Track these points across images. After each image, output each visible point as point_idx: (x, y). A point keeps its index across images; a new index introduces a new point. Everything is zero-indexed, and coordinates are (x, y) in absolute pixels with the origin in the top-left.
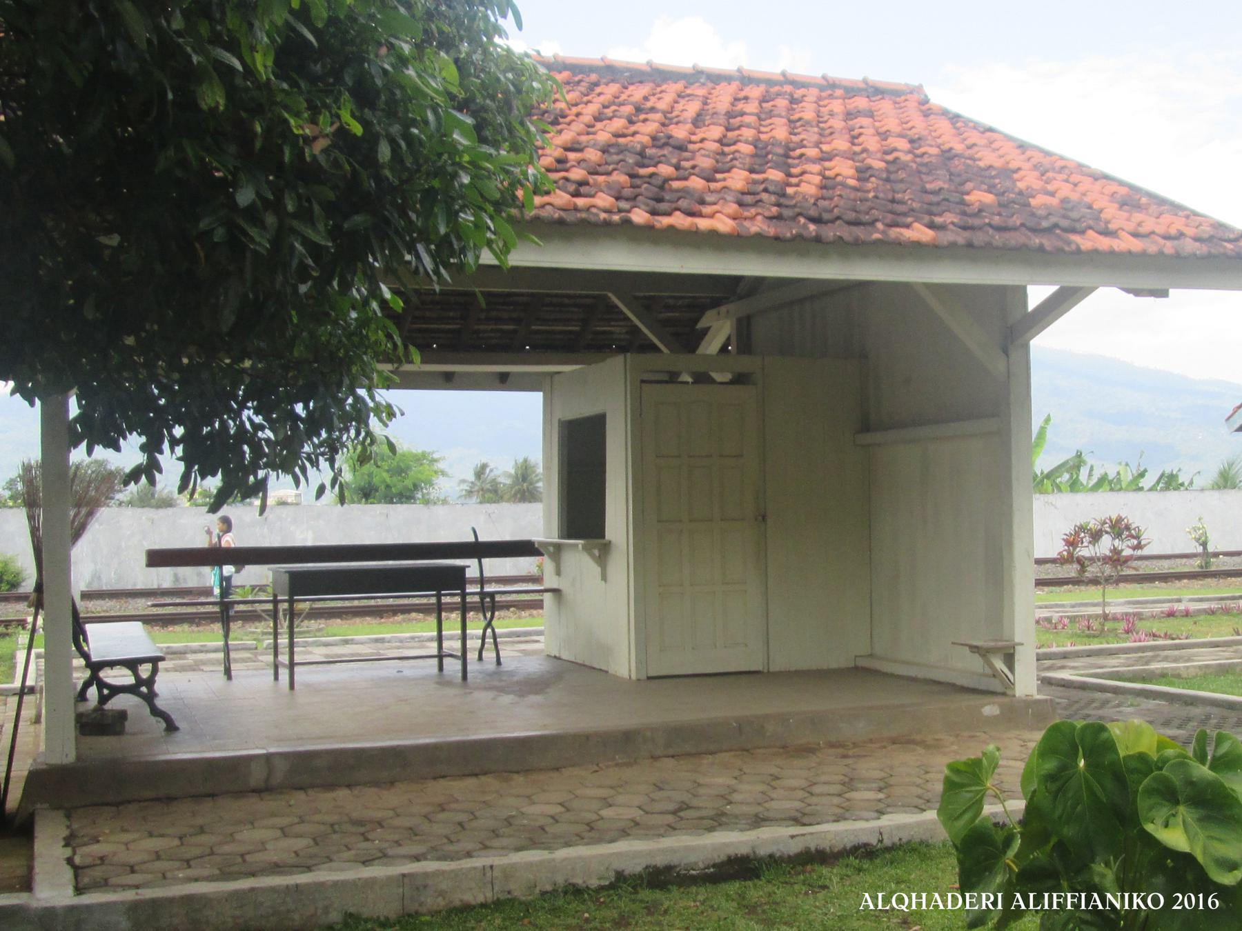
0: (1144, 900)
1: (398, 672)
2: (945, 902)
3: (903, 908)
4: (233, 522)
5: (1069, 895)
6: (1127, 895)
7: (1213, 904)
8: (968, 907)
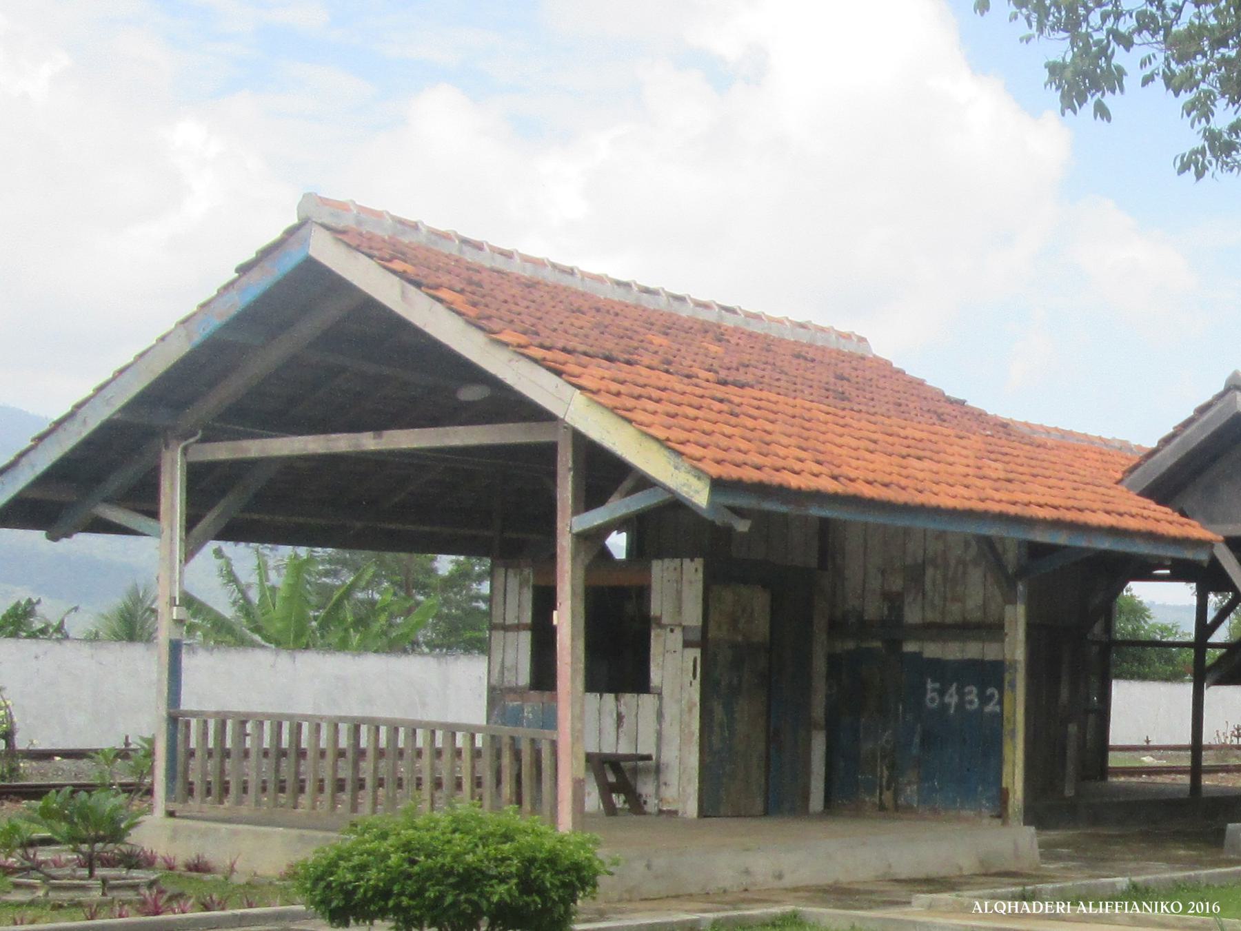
0: (1169, 907)
1: (264, 789)
2: (1031, 908)
3: (1002, 912)
4: (55, 543)
5: (1117, 903)
6: (1156, 903)
7: (1216, 909)
8: (1047, 911)
